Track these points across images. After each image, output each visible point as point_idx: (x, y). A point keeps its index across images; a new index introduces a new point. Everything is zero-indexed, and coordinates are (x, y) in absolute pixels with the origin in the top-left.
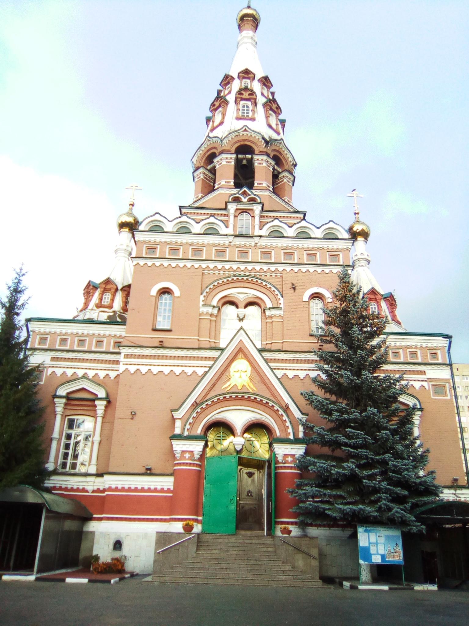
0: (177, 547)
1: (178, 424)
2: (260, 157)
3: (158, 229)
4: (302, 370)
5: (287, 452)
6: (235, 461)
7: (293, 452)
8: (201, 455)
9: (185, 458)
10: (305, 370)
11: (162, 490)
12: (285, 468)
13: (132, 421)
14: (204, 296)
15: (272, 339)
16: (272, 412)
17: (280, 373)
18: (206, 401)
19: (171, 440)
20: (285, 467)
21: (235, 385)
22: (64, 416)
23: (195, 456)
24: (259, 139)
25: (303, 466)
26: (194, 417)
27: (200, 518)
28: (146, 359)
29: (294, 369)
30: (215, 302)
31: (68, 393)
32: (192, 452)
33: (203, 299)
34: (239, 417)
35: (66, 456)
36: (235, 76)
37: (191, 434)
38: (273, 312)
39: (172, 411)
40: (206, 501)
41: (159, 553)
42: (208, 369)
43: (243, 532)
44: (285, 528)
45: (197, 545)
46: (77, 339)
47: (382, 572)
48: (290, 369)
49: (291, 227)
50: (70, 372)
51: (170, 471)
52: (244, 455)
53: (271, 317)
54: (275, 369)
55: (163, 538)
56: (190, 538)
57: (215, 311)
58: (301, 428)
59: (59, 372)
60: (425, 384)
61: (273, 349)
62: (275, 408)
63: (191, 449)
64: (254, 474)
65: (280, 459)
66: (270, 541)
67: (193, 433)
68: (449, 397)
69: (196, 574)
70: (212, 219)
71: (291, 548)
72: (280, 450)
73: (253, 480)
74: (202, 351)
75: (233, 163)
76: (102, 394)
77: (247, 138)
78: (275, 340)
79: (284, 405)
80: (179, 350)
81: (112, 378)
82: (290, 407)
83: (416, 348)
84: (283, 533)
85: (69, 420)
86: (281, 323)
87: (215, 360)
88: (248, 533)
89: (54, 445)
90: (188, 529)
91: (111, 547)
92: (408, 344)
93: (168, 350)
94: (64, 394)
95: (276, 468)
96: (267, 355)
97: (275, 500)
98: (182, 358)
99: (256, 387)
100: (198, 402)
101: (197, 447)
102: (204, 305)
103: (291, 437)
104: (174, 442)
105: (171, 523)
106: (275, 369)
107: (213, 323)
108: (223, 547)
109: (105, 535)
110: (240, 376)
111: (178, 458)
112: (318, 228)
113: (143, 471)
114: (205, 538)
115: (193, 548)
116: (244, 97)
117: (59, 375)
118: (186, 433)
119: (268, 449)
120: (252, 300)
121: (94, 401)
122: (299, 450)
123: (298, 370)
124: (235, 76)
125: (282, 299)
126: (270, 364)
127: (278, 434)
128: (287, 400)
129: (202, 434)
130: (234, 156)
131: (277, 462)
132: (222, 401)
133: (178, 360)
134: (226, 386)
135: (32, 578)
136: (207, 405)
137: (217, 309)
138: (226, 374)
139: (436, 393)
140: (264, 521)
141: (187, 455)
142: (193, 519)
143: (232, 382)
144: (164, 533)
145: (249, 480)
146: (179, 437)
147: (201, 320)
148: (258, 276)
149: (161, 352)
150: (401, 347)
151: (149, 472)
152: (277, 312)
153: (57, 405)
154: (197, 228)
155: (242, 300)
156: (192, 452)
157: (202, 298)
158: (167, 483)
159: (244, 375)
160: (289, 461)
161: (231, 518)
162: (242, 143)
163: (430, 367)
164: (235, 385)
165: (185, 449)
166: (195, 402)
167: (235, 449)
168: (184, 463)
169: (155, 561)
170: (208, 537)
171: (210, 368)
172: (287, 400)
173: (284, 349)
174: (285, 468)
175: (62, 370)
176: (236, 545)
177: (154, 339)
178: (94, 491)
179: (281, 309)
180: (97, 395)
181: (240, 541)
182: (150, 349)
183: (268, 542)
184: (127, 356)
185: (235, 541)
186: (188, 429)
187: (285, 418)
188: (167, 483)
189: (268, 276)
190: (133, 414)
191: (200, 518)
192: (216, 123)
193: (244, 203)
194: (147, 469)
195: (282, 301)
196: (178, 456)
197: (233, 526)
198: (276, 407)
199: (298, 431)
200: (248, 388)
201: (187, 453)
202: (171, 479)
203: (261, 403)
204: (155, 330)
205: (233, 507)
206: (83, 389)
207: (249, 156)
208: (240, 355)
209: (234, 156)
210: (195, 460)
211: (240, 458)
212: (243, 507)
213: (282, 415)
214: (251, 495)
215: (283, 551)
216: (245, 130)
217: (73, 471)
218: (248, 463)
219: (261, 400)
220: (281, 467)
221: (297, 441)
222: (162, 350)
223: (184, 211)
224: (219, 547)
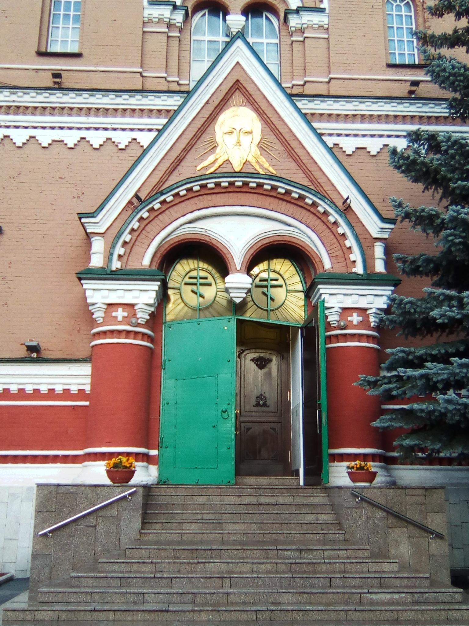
0: (92, 520)
4: (372, 136)
5: (349, 303)
6: (228, 328)
8: (152, 315)
10: (381, 136)
11: (66, 394)
12: (345, 337)
15: (305, 76)
16: (312, 219)
18: (162, 194)
19: (80, 279)
20: (345, 335)
21: (228, 161)
23: (139, 315)
25: (399, 324)
26: (133, 230)
27: (154, 452)
28: (24, 114)
29: (356, 135)
32: (363, 311)
34: (237, 231)
37: (129, 267)
38: (307, 18)
39: (81, 215)
40: (168, 417)
41: (45, 535)
42: (154, 134)
43: (251, 480)
44: (361, 468)
45: (145, 515)
48: (347, 135)
51: (84, 353)
52: (251, 315)
53: (301, 31)
55: (52, 499)
56: (125, 497)
57: (179, 17)
58: (379, 250)
61: (306, 92)
62: (320, 209)
63: (128, 299)
64: (270, 361)
65: (333, 318)
66: (319, 498)
67: (133, 265)
69: (131, 598)
71: (379, 514)
73: (269, 374)
74: (151, 96)
78: (310, 76)
79: (340, 204)
80: (99, 95)
82: (352, 205)
84: (354, 481)
86: (323, 43)
87: (172, 115)
88: (263, 481)
90: (121, 474)
93: (72, 95)
97: (329, 407)
99: (273, 166)
100: (143, 196)
101: (144, 295)
103: (359, 269)
104: (88, 285)
105: (86, 463)
107: (175, 43)
108: (209, 516)
110: (238, 140)
111: (101, 320)
113: (22, 353)
114: (165, 496)
115: (132, 523)
118: (116, 265)
119: (302, 303)
122: (376, 299)
123: (364, 136)
127: (328, 265)
128: (345, 188)
129: (154, 267)
132: (198, 195)
133: (97, 116)
134: (207, 163)
136: (164, 202)
137: (183, 12)
138: (206, 137)
140: (296, 457)
141: (120, 314)
142: (137, 454)
143: (220, 156)
144: (58, 485)
145: (261, 373)
146: (105, 274)
147: (148, 36)
149: (57, 99)
151: (34, 354)
152: (315, 19)
156: (132, 306)
158: (77, 377)
159: (245, 140)
160: (355, 323)
161: (224, 449)
164: (228, 161)
165: (114, 298)
166: (136, 196)
167: (230, 301)
168: (112, 332)
169: (35, 556)
170: (171, 492)
171: (160, 132)
172: (345, 188)
173: (332, 93)
174: (345, 337)
176: (242, 509)
177: (41, 73)
179: (322, 10)
181: (248, 500)
182: (33, 93)
183: (316, 500)
185: (237, 500)
186: (120, 256)
187: (343, 228)
188: (77, 377)
191: (154, 452)
194: (32, 349)
196: (98, 315)
197: (230, 466)
198: (323, 206)
199: (373, 258)
201: (120, 310)
202: (86, 369)
203: (286, 198)
204: (43, 54)
205: (229, 427)
208: (238, 97)
210: (139, 325)
211: (241, 323)
212: (248, 429)
213: (335, 223)
214: (265, 405)
215: (361, 521)
218: (261, 338)
219: (288, 193)
220: (336, 336)
221: (369, 279)
222: (59, 94)
224: (199, 516)
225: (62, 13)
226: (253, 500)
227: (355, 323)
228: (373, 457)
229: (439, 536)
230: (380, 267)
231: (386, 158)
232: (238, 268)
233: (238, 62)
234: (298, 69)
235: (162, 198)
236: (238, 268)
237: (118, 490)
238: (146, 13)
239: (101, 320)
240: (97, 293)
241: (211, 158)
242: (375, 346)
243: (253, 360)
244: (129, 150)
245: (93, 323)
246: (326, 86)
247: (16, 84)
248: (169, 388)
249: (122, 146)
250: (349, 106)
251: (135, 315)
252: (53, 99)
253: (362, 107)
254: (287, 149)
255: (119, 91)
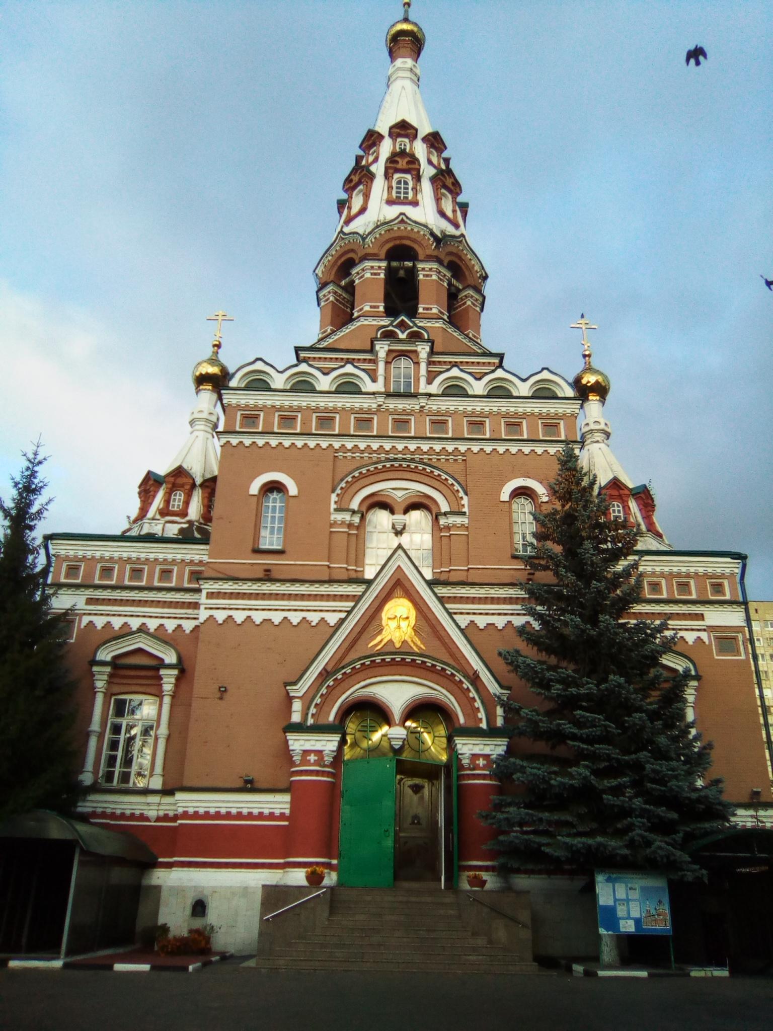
1: (297, 706)
2: (427, 266)
3: (547, 394)
5: (477, 750)
7: (487, 751)
8: (335, 758)
9: (308, 763)
13: (220, 702)
14: (338, 495)
17: (463, 621)
18: (343, 668)
19: (285, 732)
20: (474, 775)
21: (391, 641)
22: (108, 695)
23: (326, 758)
24: (424, 235)
27: (335, 862)
30: (355, 505)
31: (115, 658)
32: (319, 753)
33: (336, 499)
34: (397, 694)
35: (112, 760)
36: (384, 131)
38: (452, 520)
41: (268, 919)
42: (345, 614)
43: (406, 885)
46: (128, 567)
47: (636, 949)
49: (480, 379)
50: (117, 623)
51: (284, 785)
52: (406, 756)
53: (448, 528)
54: (455, 613)
57: (356, 519)
58: (499, 711)
59: (100, 622)
60: (704, 636)
61: (451, 580)
63: (318, 746)
64: (423, 787)
65: (465, 762)
66: (450, 899)
67: (322, 721)
68: (743, 657)
70: (349, 368)
72: (467, 747)
73: (422, 798)
75: (382, 276)
76: (170, 658)
77: (405, 234)
81: (691, 643)
83: (688, 575)
85: (116, 700)
86: (464, 538)
87: (357, 599)
88: (415, 885)
89: (93, 742)
91: (188, 911)
92: (675, 569)
94: (108, 658)
95: (460, 777)
96: (443, 591)
98: (302, 597)
100: (329, 669)
101: (328, 744)
102: (336, 510)
103: (484, 725)
104: (290, 736)
106: (455, 613)
107: (354, 539)
109: (179, 891)
110: (398, 623)
111: (298, 762)
112: (524, 380)
116: (399, 166)
117: (691, 643)
119: (445, 746)
120: (416, 500)
121: (157, 669)
122: (495, 748)
123: (493, 614)
124: (384, 131)
125: (465, 498)
126: (447, 606)
127: (462, 720)
130: (384, 264)
131: (461, 767)
134: (377, 642)
135: (58, 964)
138: (375, 623)
139: (721, 651)
141: (312, 758)
143: (385, 636)
145: (416, 798)
146: (300, 728)
148: (425, 461)
149: (267, 588)
150: (662, 575)
151: (249, 786)
152: (459, 520)
153: (165, 680)
154: (324, 383)
155: (399, 500)
157: (334, 497)
159: (404, 624)
160: (481, 765)
162: (398, 242)
163: (711, 608)
164: (391, 641)
166: (324, 669)
167: (391, 747)
169: (261, 934)
171: (349, 613)
175: (695, 635)
177: (255, 567)
178: (158, 819)
180: (162, 660)
181: (400, 899)
184: (211, 595)
187: (473, 694)
189: (434, 460)
190: (223, 691)
191: (335, 862)
192: (355, 210)
193: (401, 341)
194: (247, 782)
195: (465, 501)
196: (297, 758)
197: (390, 873)
199: (495, 716)
200: (412, 645)
202: (287, 798)
204: (257, 551)
205: (389, 843)
206: (140, 651)
207: (410, 264)
208: (399, 591)
209: (384, 264)
210: (325, 766)
211: (399, 762)
214: (419, 823)
216: (402, 221)
217: (124, 786)
221: (492, 732)
223: (303, 355)
225: (270, 515)
226: (405, 899)
227: (481, 765)
228: (486, 869)
229: (524, 926)
230: (500, 722)
231: (510, 632)
232: (397, 722)
233: (399, 566)
234: (445, 557)
235: (343, 671)
236: (397, 722)
237: (314, 890)
238: (333, 517)
239: (298, 762)
240: (296, 742)
241: (379, 638)
242: (494, 782)
243: (410, 786)
244: (318, 627)
245: (292, 763)
246: (465, 573)
247: (236, 575)
248: (346, 811)
249: (313, 624)
250: (482, 591)
251: (323, 758)
252: (264, 587)
253: (492, 591)
254: (433, 631)
255: (312, 582)
